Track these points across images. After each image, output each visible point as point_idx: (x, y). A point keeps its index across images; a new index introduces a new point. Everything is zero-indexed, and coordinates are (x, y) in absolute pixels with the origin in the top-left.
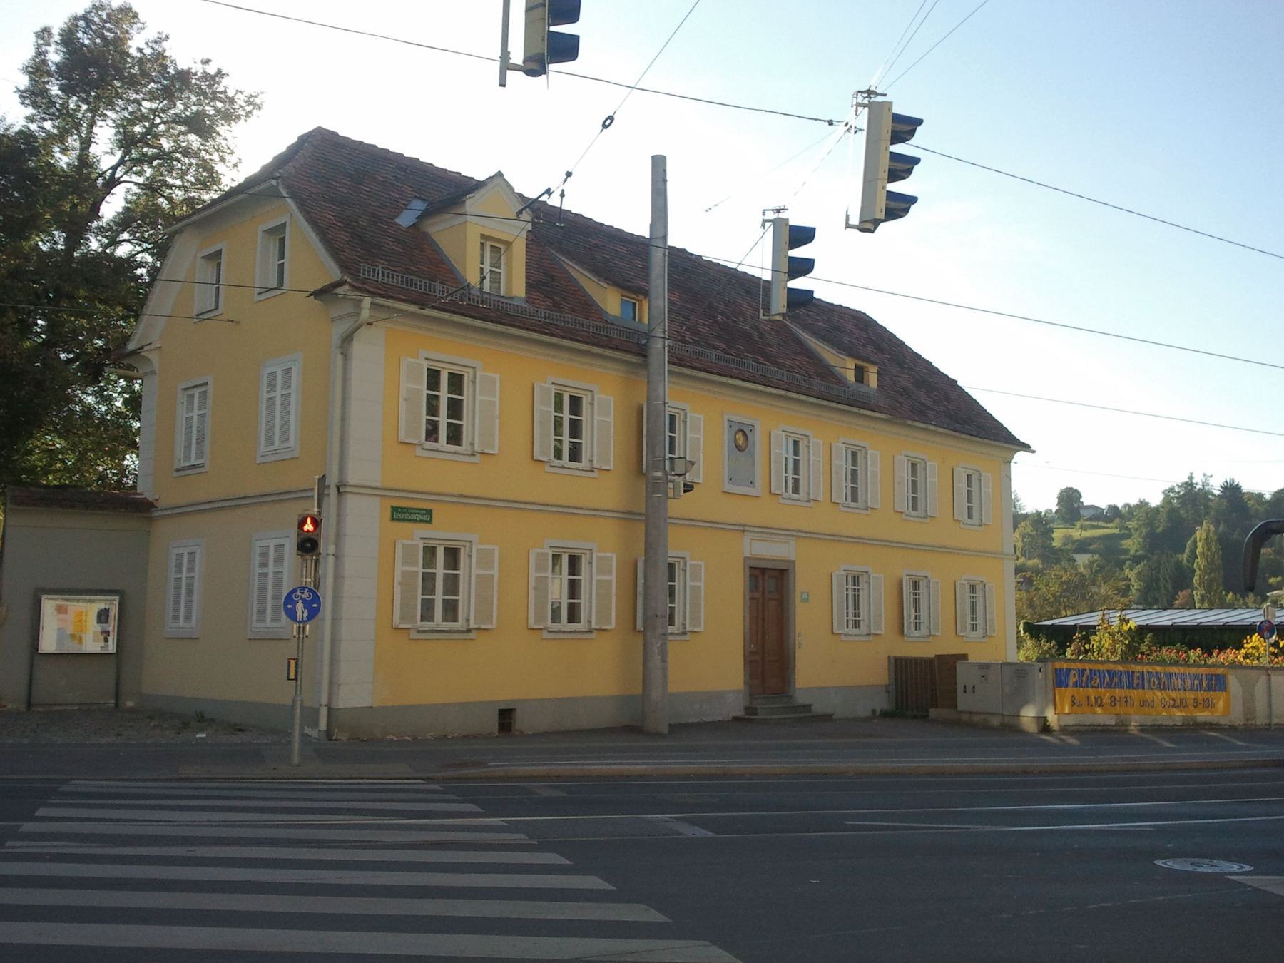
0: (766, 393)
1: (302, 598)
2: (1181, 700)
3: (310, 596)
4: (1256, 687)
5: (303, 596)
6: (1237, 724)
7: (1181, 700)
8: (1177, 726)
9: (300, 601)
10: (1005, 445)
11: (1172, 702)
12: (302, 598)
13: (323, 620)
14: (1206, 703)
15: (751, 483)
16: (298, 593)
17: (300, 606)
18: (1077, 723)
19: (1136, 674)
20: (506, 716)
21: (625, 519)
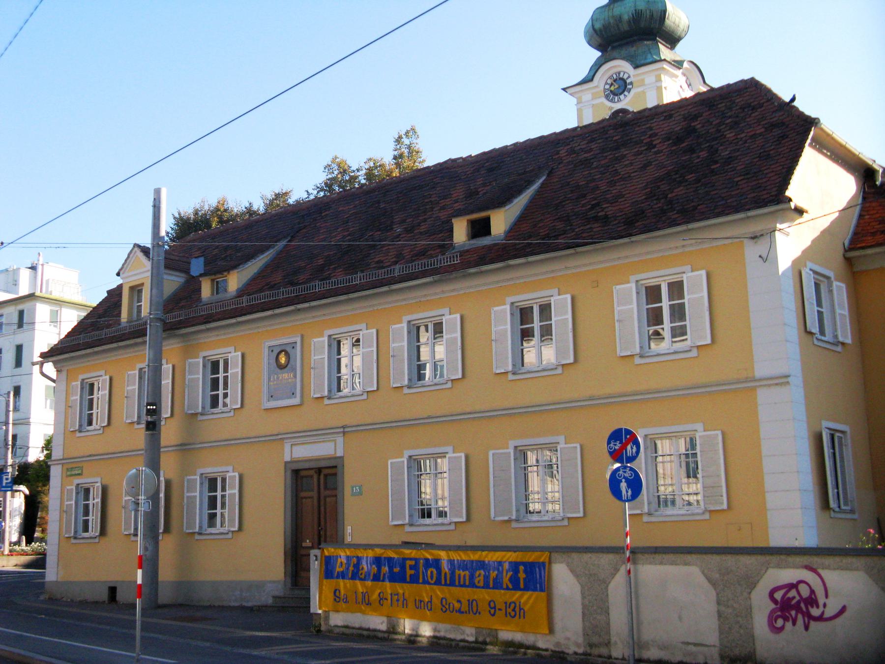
0: (276, 315)
1: (625, 478)
2: (470, 603)
3: (632, 474)
4: (612, 586)
5: (626, 475)
6: (571, 651)
7: (470, 603)
8: (467, 642)
9: (623, 480)
10: (691, 226)
11: (457, 605)
12: (625, 478)
13: (643, 495)
14: (509, 610)
15: (293, 394)
16: (621, 472)
17: (623, 485)
18: (346, 624)
19: (408, 563)
20: (113, 590)
21: (180, 450)
